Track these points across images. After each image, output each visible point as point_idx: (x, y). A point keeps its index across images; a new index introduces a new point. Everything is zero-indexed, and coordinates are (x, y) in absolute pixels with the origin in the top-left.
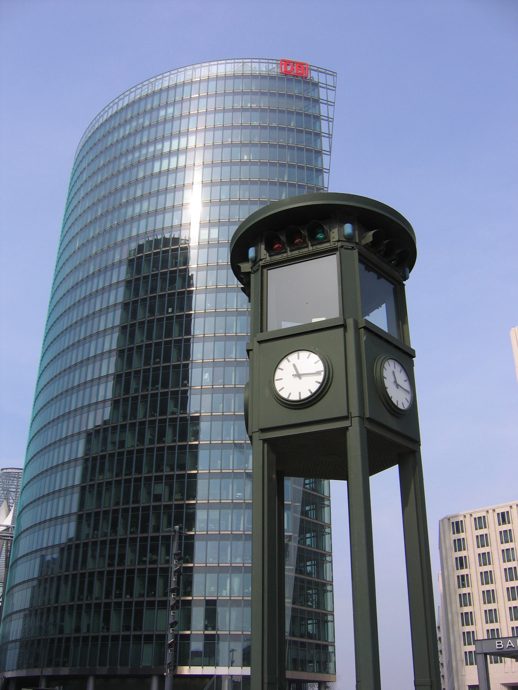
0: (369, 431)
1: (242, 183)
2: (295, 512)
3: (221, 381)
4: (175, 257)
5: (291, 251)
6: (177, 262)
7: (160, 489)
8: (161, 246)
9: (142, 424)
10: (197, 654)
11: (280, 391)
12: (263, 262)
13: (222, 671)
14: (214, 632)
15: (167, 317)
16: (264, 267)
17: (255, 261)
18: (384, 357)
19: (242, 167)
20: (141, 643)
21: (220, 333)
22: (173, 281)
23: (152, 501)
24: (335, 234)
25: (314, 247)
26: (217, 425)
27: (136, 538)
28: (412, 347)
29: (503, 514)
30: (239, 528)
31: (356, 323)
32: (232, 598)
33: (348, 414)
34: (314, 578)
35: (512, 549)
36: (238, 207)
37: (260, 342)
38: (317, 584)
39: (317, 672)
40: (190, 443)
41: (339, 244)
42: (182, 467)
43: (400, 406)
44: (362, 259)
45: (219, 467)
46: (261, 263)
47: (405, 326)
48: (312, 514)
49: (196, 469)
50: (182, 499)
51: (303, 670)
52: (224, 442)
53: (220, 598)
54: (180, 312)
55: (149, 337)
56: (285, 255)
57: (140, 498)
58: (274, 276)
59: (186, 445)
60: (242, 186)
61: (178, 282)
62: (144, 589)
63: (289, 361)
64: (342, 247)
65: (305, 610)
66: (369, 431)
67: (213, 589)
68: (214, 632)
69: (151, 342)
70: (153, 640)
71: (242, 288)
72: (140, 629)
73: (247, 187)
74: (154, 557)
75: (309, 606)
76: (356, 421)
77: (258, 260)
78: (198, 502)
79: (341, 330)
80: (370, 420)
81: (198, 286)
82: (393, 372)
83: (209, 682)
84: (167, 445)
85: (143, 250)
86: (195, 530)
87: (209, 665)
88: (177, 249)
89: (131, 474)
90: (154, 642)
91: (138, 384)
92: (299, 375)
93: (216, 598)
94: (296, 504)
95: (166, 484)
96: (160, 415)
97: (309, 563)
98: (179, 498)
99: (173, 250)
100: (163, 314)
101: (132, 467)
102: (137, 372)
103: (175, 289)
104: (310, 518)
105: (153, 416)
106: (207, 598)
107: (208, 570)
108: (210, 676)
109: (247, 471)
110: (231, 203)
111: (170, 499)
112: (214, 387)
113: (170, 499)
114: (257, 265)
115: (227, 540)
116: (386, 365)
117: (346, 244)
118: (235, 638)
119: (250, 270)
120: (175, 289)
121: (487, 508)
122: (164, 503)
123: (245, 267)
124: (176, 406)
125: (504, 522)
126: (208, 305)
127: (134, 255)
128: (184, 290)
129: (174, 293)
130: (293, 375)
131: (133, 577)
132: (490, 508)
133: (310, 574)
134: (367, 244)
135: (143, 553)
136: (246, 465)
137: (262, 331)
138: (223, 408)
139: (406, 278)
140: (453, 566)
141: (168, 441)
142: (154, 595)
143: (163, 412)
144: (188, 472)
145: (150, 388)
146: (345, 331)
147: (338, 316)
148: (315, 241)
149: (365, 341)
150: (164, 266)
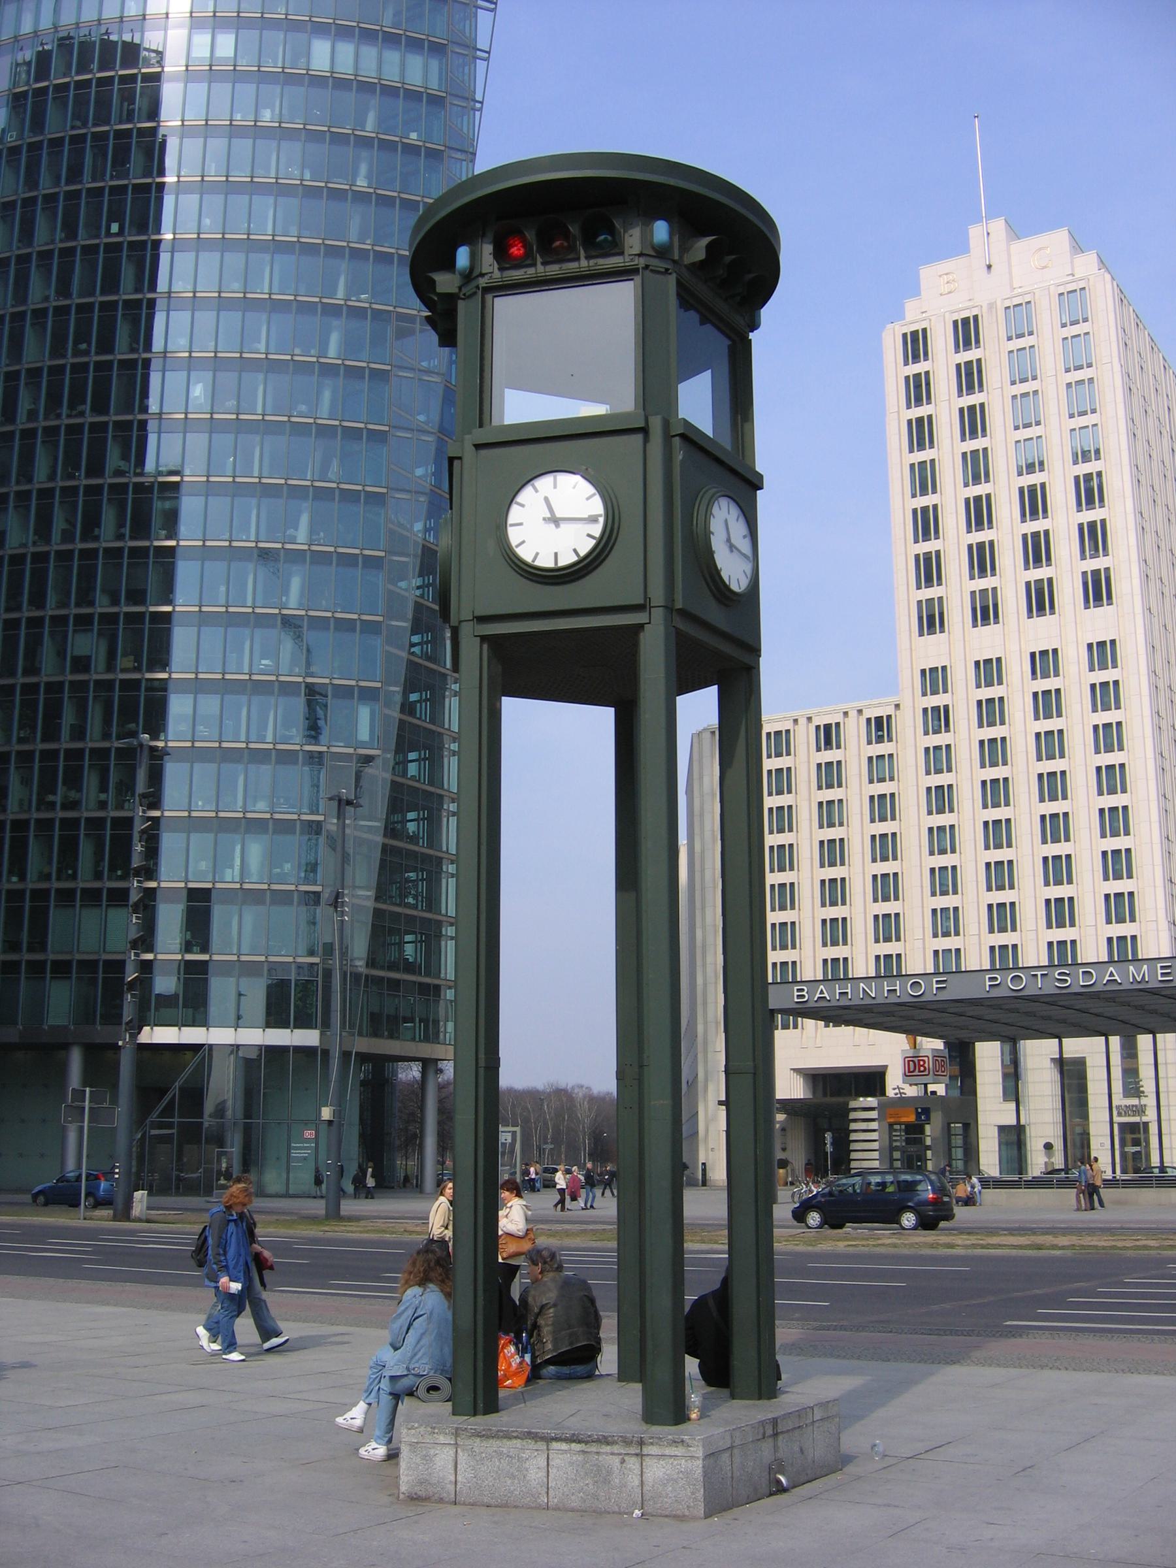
0: (679, 633)
2: (387, 704)
3: (232, 403)
4: (128, 97)
5: (544, 264)
6: (134, 110)
7: (84, 644)
8: (95, 66)
9: (46, 494)
10: (166, 1001)
13: (219, 1036)
14: (205, 957)
15: (106, 244)
16: (487, 290)
17: (469, 276)
20: (44, 978)
21: (234, 291)
22: (121, 159)
23: (68, 669)
24: (633, 240)
25: (592, 262)
26: (219, 505)
27: (32, 752)
29: (828, 727)
30: (265, 736)
31: (666, 424)
32: (246, 886)
34: (422, 848)
35: (840, 801)
37: (478, 447)
38: (426, 858)
39: (420, 1041)
40: (156, 543)
41: (642, 262)
42: (137, 596)
43: (734, 587)
44: (686, 299)
45: (223, 601)
46: (483, 282)
47: (747, 426)
48: (424, 710)
49: (169, 602)
50: (138, 669)
51: (391, 1036)
52: (235, 544)
53: (218, 885)
54: (139, 234)
55: (64, 290)
56: (531, 271)
57: (41, 662)
58: (508, 311)
59: (148, 548)
61: (136, 158)
62: (50, 863)
63: (536, 491)
64: (647, 267)
65: (400, 914)
66: (679, 633)
67: (203, 865)
68: (205, 957)
69: (67, 302)
70: (71, 973)
71: (427, 317)
72: (43, 947)
74: (73, 795)
75: (408, 906)
76: (658, 615)
77: (475, 274)
78: (174, 676)
79: (639, 437)
80: (684, 613)
81: (183, 173)
83: (193, 1061)
84: (104, 545)
85: (49, 75)
86: (166, 737)
87: (193, 1024)
88: (133, 78)
89: (18, 608)
90: (74, 976)
91: (36, 400)
92: (555, 521)
93: (209, 886)
94: (392, 688)
95: (100, 634)
96: (88, 476)
97: (411, 815)
98: (130, 665)
99: (124, 79)
100: (98, 236)
101: (22, 594)
102: (35, 373)
103: (126, 176)
104: (420, 719)
105: (71, 477)
106: (191, 885)
107: (192, 825)
108: (196, 1048)
109: (285, 612)
111: (110, 667)
112: (215, 416)
113: (110, 667)
114: (473, 284)
115: (238, 761)
116: (715, 510)
117: (655, 263)
118: (249, 969)
120: (126, 176)
121: (795, 714)
122: (95, 677)
123: (445, 282)
124: (125, 457)
125: (828, 744)
126: (207, 222)
127: (27, 83)
128: (149, 180)
129: (126, 186)
130: (544, 519)
131: (26, 838)
132: (801, 714)
133: (414, 839)
134: (693, 264)
135: (48, 786)
136: (284, 599)
137: (481, 426)
138: (235, 466)
139: (754, 325)
140: (713, 831)
141: (107, 538)
142: (74, 877)
143: (96, 468)
144: (153, 609)
145: (65, 411)
146: (646, 440)
148: (595, 248)
149: (682, 462)
150: (103, 117)
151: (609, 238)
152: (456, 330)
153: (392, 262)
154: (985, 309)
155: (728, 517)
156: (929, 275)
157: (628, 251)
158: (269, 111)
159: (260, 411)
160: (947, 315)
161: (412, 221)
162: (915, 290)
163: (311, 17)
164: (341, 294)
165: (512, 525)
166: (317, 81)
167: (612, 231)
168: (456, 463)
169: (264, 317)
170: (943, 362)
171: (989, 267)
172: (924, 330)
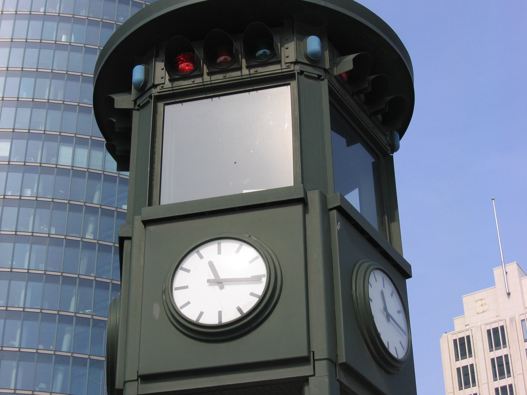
1: (55, 76)
11: (182, 307)
12: (158, 89)
16: (159, 98)
17: (143, 88)
18: (367, 264)
19: (57, 52)
24: (289, 52)
25: (252, 71)
28: (406, 256)
31: (324, 199)
33: (309, 351)
36: (45, 114)
37: (147, 223)
41: (297, 68)
43: (392, 351)
46: (155, 92)
56: (198, 80)
58: (178, 118)
60: (54, 81)
63: (201, 257)
64: (301, 73)
73: (62, 83)
76: (322, 367)
79: (298, 208)
80: (346, 368)
82: (382, 292)
110: (35, 104)
114: (148, 94)
116: (372, 280)
117: (308, 69)
119: (131, 106)
123: (122, 101)
130: (209, 281)
137: (150, 204)
139: (395, 148)
146: (306, 210)
147: (291, 184)
151: (268, 52)
152: (130, 129)
153: (108, 289)
154: (508, 322)
155: (383, 289)
156: (469, 301)
157: (284, 60)
158: (30, 190)
159: (12, 387)
160: (483, 326)
161: (96, 58)
162: (460, 312)
163: (60, 132)
164: (72, 308)
165: (177, 289)
166: (62, 172)
167: (271, 46)
168: (126, 243)
169: (19, 323)
170: (482, 358)
171: (509, 294)
172: (468, 337)
